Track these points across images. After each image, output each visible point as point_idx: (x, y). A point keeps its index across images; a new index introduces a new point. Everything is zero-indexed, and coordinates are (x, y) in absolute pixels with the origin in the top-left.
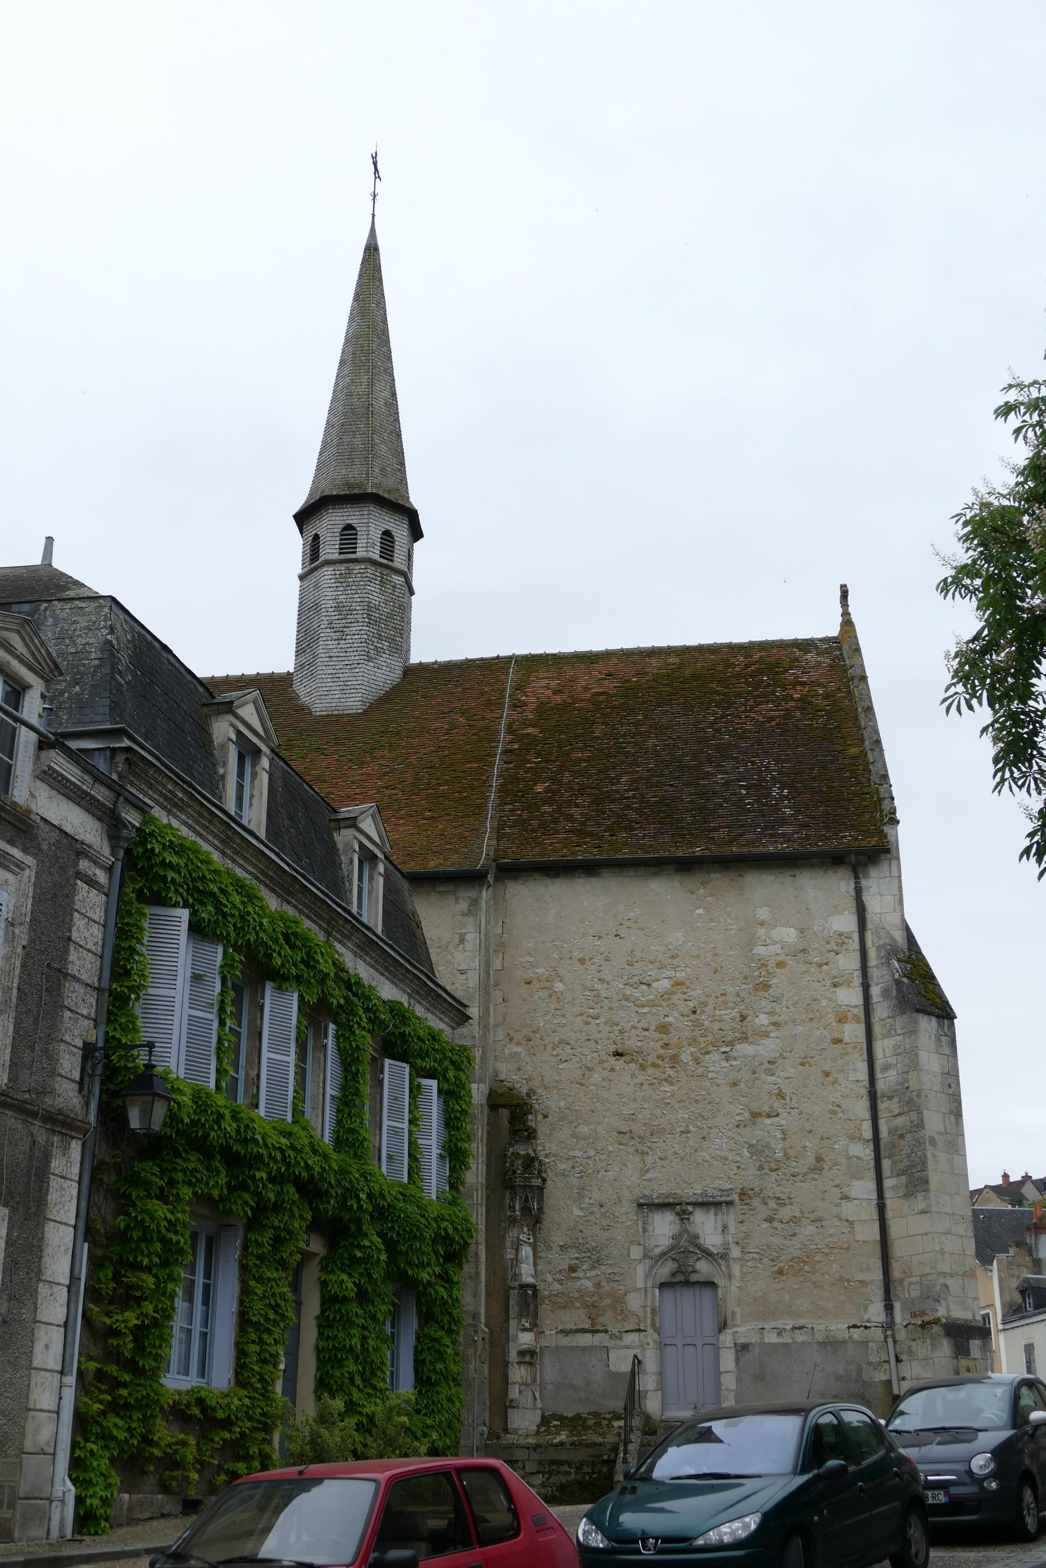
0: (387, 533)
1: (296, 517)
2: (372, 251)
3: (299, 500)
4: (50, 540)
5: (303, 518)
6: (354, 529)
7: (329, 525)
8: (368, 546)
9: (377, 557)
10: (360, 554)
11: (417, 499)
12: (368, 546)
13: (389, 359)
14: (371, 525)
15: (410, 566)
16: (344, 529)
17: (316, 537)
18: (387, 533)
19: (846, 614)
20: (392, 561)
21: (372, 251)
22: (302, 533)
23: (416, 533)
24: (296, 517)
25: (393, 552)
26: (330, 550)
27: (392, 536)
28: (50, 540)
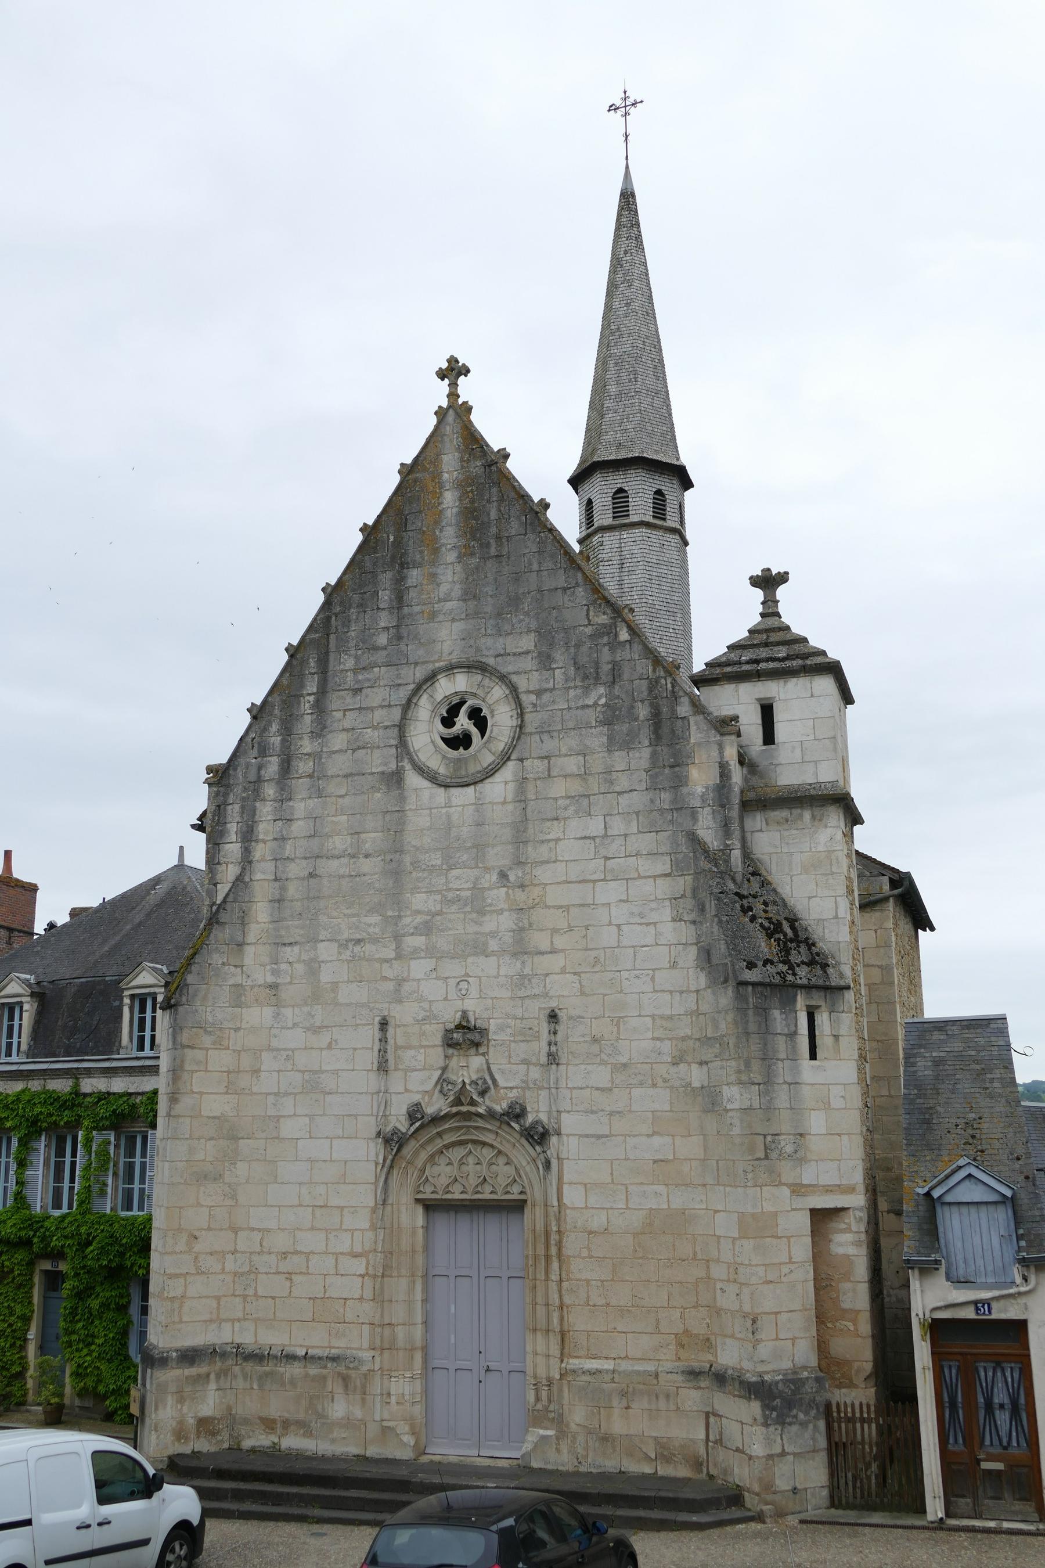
0: (659, 492)
1: (570, 481)
2: (628, 199)
3: (571, 465)
4: (181, 848)
5: (576, 481)
6: (626, 492)
7: (601, 488)
8: (640, 508)
9: (651, 520)
10: (634, 518)
11: (687, 458)
12: (640, 508)
13: (650, 314)
14: (640, 489)
15: (682, 522)
16: (616, 493)
17: (590, 502)
18: (659, 492)
19: (627, 167)
20: (664, 519)
21: (628, 199)
22: (577, 493)
23: (687, 483)
24: (570, 481)
25: (664, 501)
26: (603, 517)
27: (663, 495)
28: (181, 848)
